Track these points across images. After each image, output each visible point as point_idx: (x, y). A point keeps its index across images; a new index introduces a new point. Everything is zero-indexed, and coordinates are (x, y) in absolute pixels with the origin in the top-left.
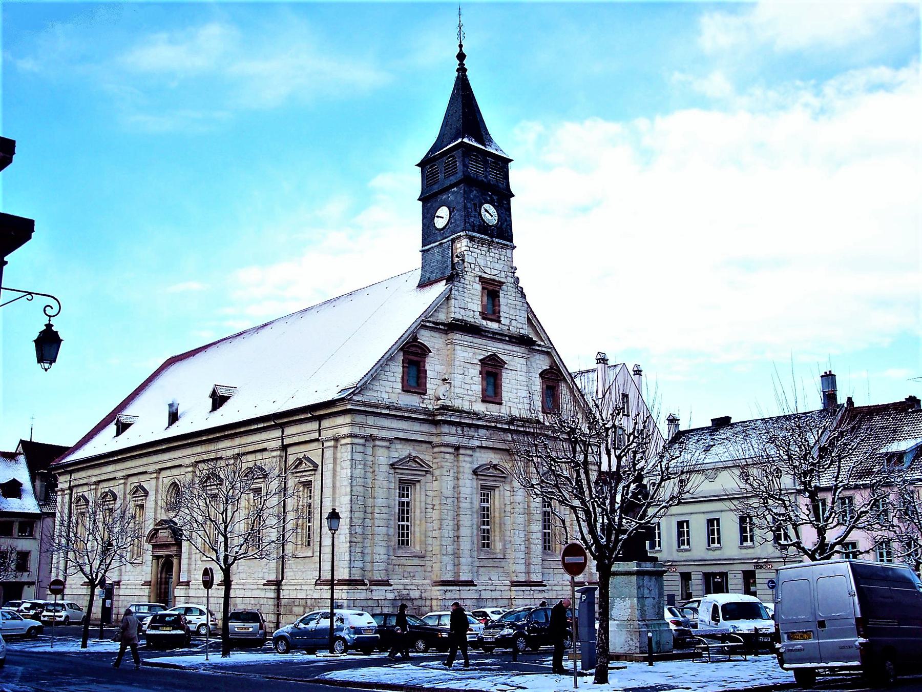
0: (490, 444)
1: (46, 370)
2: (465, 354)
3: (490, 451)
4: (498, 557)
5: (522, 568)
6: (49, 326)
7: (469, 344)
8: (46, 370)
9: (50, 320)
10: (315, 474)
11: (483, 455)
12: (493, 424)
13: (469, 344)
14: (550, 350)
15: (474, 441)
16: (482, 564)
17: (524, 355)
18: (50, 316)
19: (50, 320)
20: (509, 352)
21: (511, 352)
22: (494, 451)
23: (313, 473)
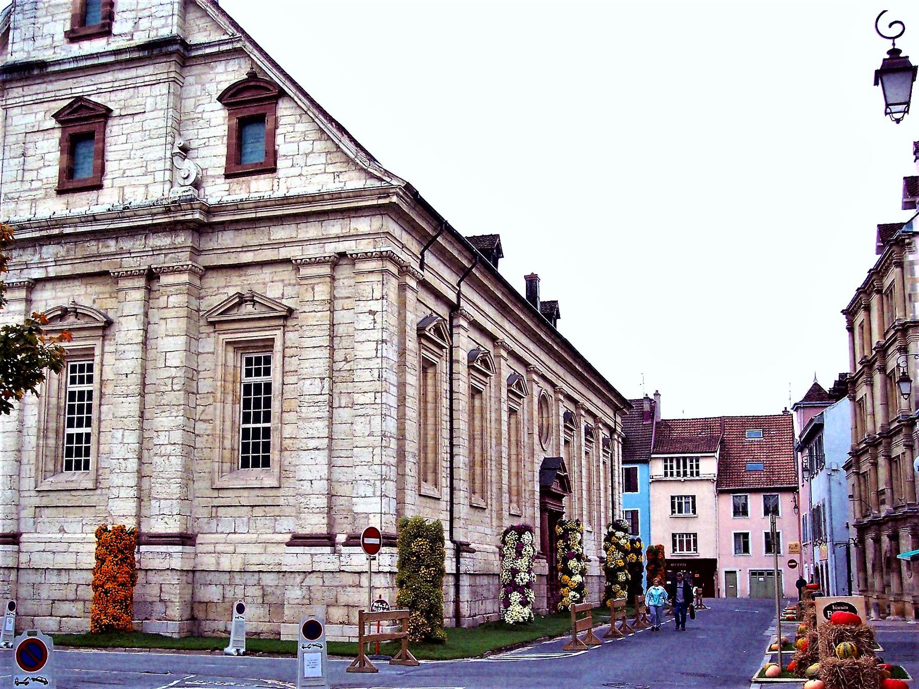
0: (66, 270)
1: (898, 121)
2: (30, 119)
3: (77, 283)
4: (82, 486)
5: (130, 507)
6: (894, 52)
7: (34, 97)
8: (898, 121)
9: (894, 44)
10: (284, 326)
11: (59, 294)
12: (56, 231)
13: (34, 97)
14: (238, 45)
15: (33, 271)
16: (45, 501)
17: (158, 77)
18: (893, 38)
19: (894, 44)
20: (123, 83)
21: (129, 82)
22: (85, 281)
23: (281, 322)
